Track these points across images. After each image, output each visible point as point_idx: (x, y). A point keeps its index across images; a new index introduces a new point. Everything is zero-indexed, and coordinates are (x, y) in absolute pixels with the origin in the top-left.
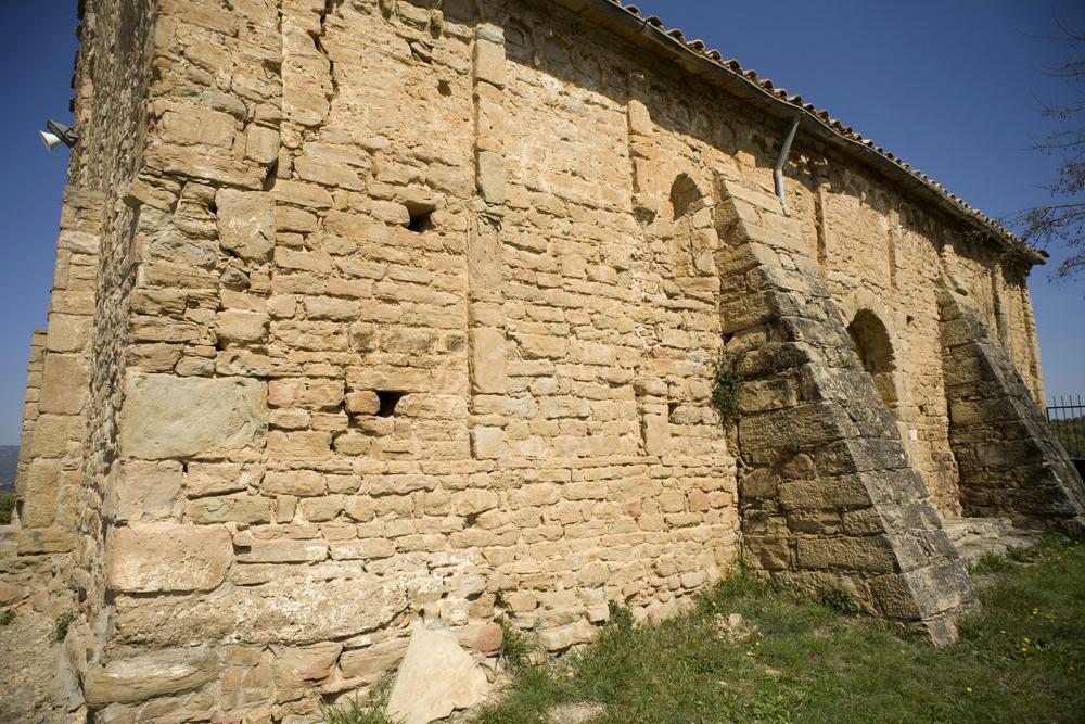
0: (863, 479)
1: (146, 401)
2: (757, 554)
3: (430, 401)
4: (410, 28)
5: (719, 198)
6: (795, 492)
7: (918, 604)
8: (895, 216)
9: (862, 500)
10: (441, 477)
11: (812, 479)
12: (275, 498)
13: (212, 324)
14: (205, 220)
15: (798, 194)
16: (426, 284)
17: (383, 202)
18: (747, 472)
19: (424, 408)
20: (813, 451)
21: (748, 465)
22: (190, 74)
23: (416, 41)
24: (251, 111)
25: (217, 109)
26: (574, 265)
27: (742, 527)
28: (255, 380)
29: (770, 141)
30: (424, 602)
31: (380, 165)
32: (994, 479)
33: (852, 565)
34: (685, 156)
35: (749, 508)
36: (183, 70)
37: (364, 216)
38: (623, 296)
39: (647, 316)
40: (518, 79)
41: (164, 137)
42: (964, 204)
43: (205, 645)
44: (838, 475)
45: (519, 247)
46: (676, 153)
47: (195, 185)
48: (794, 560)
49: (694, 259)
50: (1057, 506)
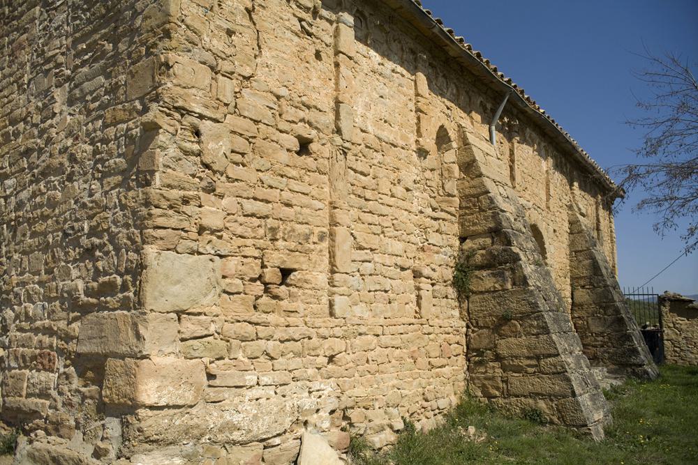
0: (554, 338)
1: (160, 271)
2: (479, 387)
3: (308, 277)
4: (301, 11)
5: (461, 143)
6: (506, 346)
7: (586, 416)
8: (551, 161)
9: (552, 351)
10: (316, 330)
11: (520, 337)
12: (228, 341)
13: (196, 217)
14: (193, 142)
15: (501, 143)
16: (307, 194)
17: (285, 134)
18: (473, 332)
19: (306, 281)
20: (521, 319)
21: (475, 327)
22: (188, 36)
23: (304, 20)
24: (219, 66)
25: (201, 63)
26: (385, 187)
27: (468, 369)
28: (218, 257)
29: (489, 106)
30: (306, 416)
31: (285, 108)
32: (598, 341)
33: (544, 393)
34: (444, 113)
35: (474, 356)
36: (183, 33)
37: (275, 144)
38: (409, 208)
39: (421, 223)
40: (357, 52)
41: (174, 81)
42: (587, 155)
43: (191, 444)
44: (537, 335)
45: (355, 171)
46: (442, 112)
47: (190, 117)
48: (505, 391)
49: (443, 184)
50: (634, 359)
